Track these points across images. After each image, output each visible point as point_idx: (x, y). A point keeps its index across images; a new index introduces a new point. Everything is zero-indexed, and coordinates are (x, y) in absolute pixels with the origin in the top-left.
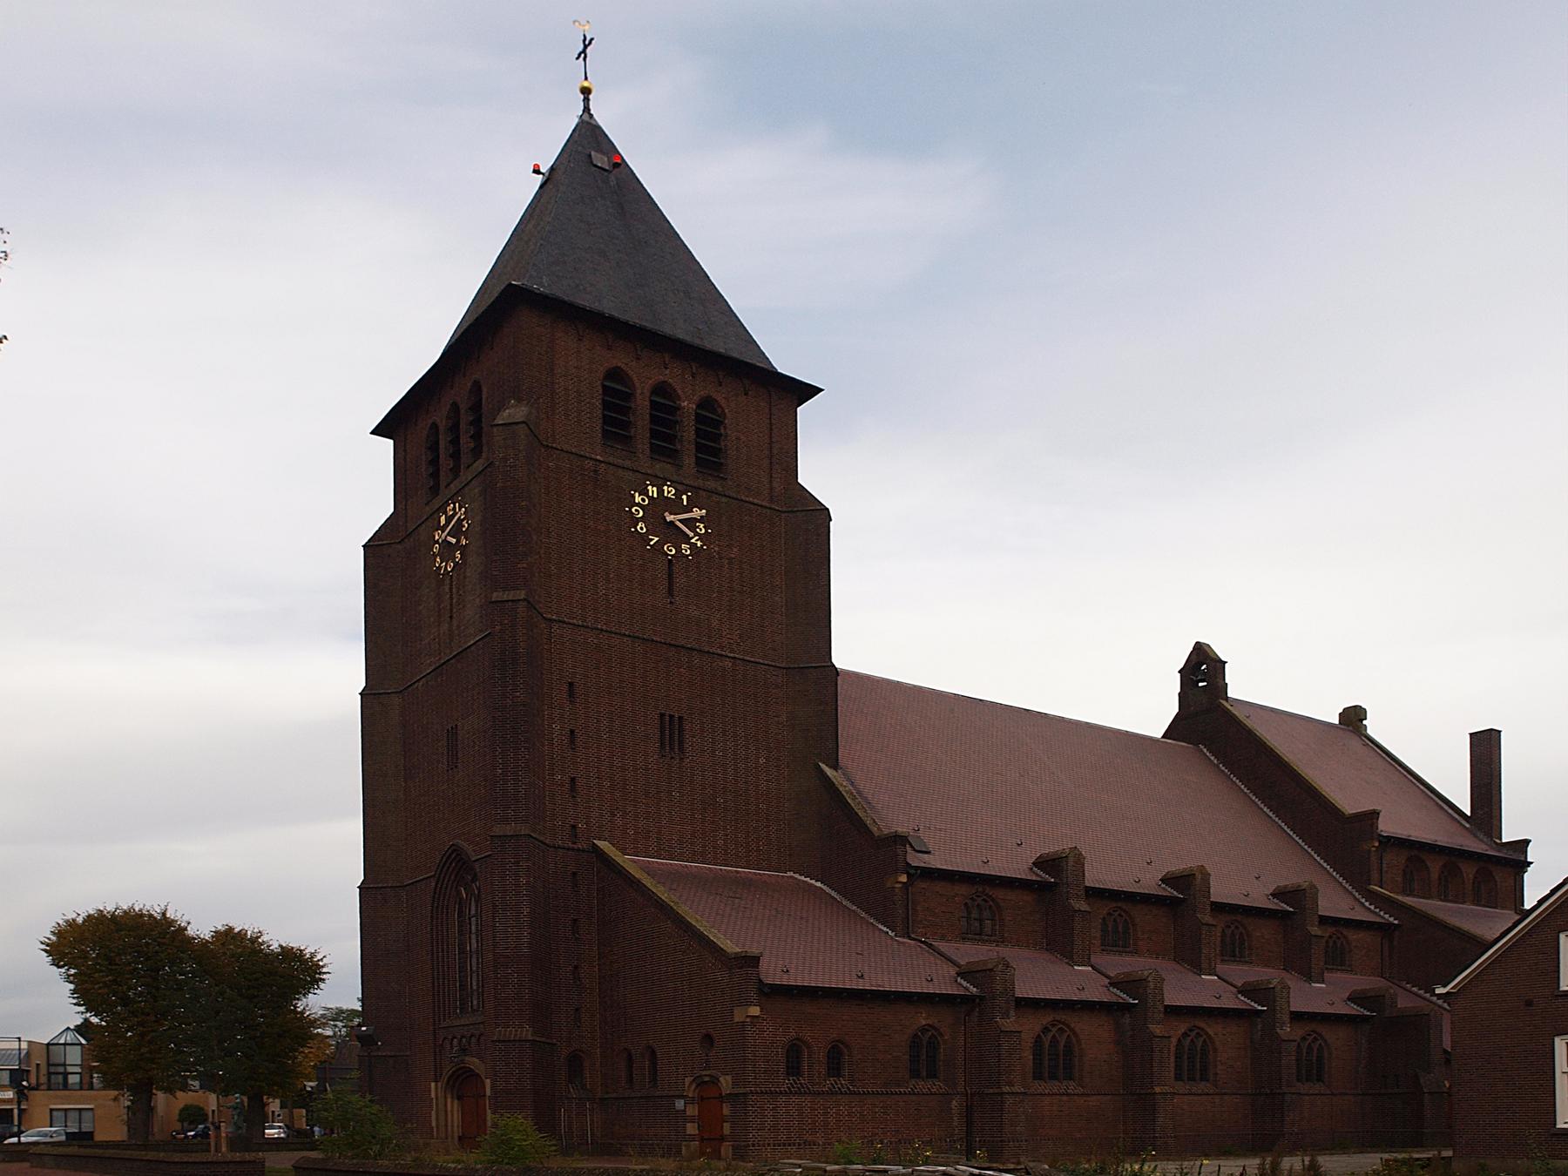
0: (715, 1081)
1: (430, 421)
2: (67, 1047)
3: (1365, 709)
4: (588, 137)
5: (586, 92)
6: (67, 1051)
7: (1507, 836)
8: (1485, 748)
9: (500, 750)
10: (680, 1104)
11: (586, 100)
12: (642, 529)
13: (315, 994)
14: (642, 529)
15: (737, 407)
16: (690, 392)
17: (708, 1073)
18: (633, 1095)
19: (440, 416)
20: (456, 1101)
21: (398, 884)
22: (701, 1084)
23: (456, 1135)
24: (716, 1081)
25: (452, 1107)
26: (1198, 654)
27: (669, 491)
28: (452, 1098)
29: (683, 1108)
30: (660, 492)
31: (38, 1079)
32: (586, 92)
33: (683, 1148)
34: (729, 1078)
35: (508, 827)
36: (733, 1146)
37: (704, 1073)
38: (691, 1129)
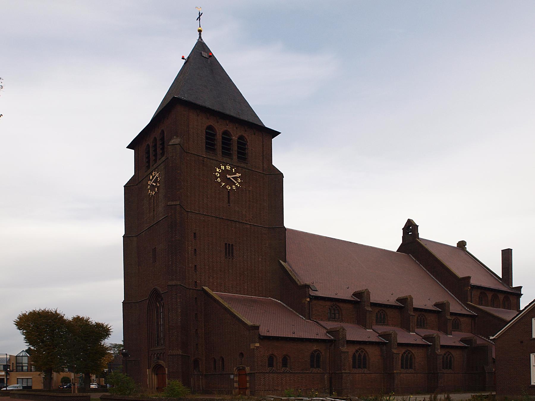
0: (244, 369)
4: (201, 47)
5: (200, 31)
10: (232, 377)
11: (200, 34)
12: (219, 180)
13: (107, 339)
14: (219, 180)
17: (242, 366)
23: (156, 387)
28: (154, 374)
32: (200, 31)
34: (249, 368)
36: (250, 391)
38: (236, 385)
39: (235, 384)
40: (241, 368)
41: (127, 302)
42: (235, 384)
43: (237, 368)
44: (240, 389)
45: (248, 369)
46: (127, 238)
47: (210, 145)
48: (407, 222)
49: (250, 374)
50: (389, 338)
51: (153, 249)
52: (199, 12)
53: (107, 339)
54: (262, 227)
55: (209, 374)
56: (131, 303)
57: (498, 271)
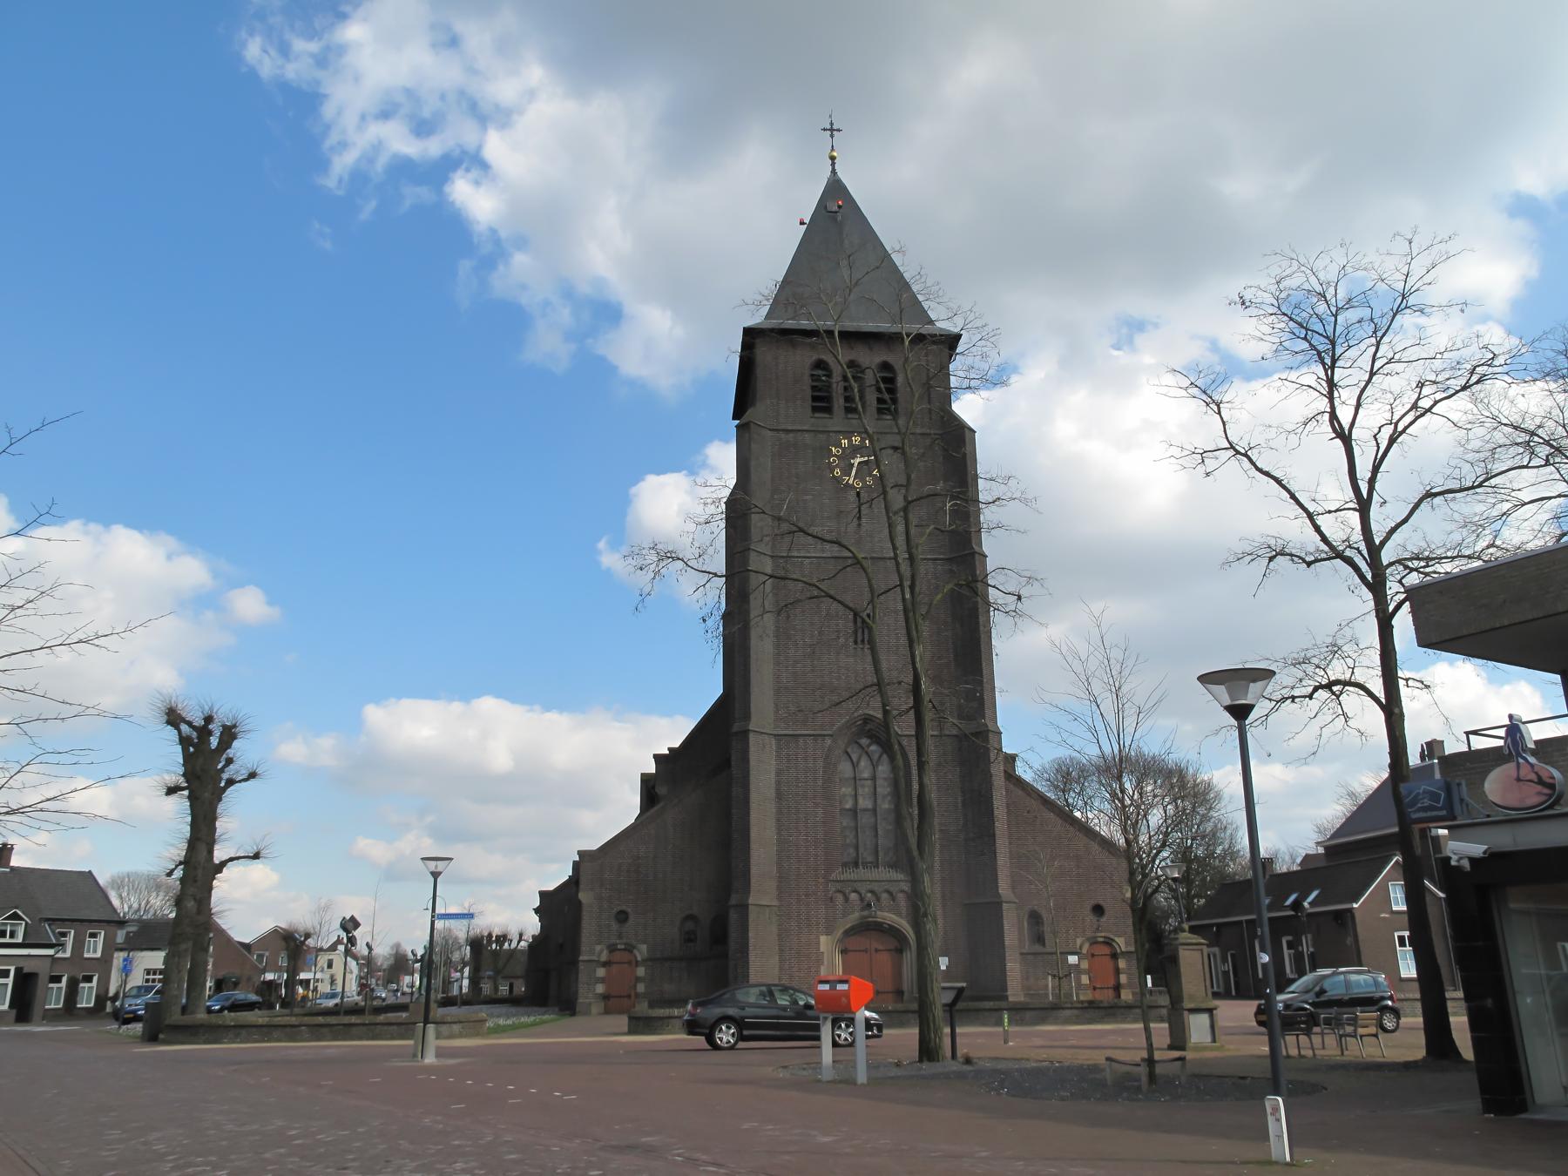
2: (438, 911)
4: (835, 189)
6: (453, 910)
7: (667, 752)
10: (1073, 959)
11: (833, 164)
12: (837, 473)
14: (837, 473)
15: (907, 364)
16: (870, 358)
17: (1103, 934)
22: (1094, 942)
24: (1110, 942)
27: (856, 440)
30: (850, 441)
32: (833, 158)
38: (1085, 979)
44: (1095, 988)
46: (365, 1028)
47: (821, 402)
52: (132, 716)
54: (929, 715)
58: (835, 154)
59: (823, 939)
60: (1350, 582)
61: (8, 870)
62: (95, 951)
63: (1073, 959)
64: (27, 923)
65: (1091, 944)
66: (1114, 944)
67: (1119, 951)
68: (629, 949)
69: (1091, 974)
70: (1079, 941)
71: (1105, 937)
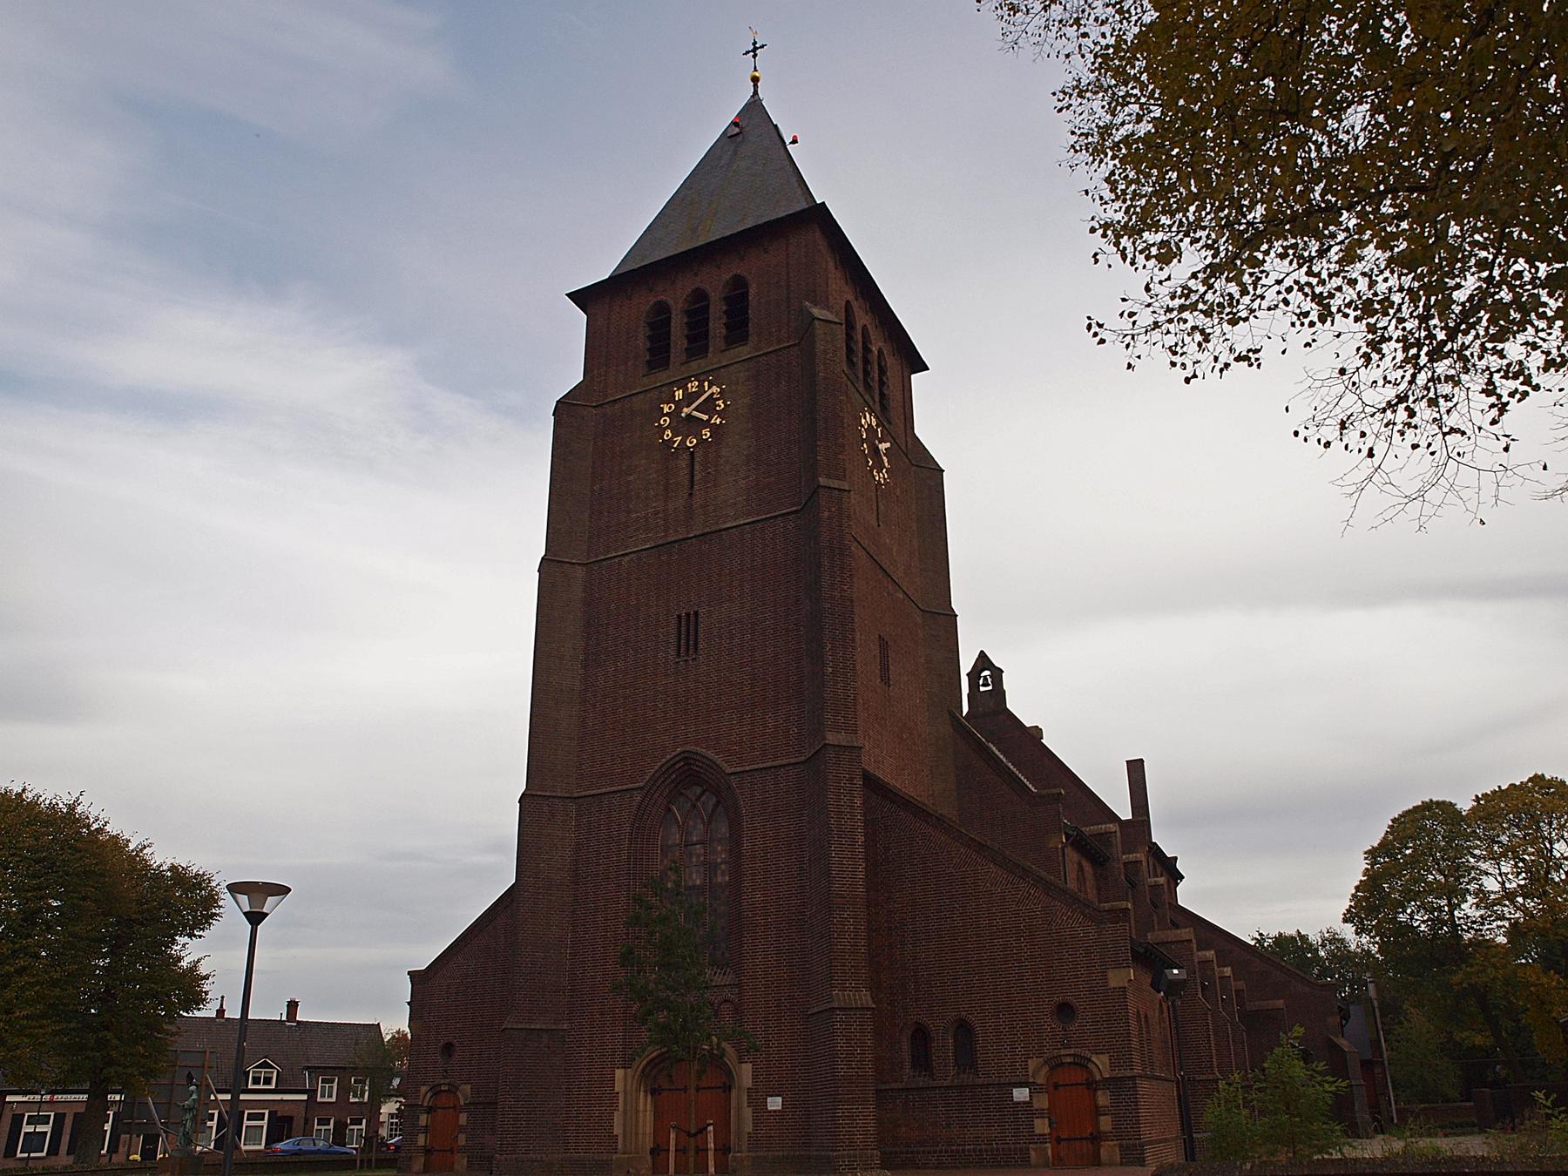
0: (1082, 1063)
1: (653, 300)
3: (1041, 729)
4: (755, 107)
5: (755, 80)
8: (1136, 769)
9: (830, 646)
10: (1021, 1094)
11: (755, 86)
12: (668, 435)
13: (200, 937)
14: (668, 435)
18: (934, 1084)
19: (676, 296)
20: (649, 1097)
21: (567, 795)
22: (1056, 1065)
23: (648, 1148)
25: (645, 1104)
26: (983, 662)
28: (645, 1091)
29: (1028, 1099)
31: (1093, 1062)
32: (755, 80)
33: (1032, 1153)
34: (1105, 1058)
35: (839, 736)
36: (1121, 1146)
37: (1063, 1052)
38: (1041, 1126)
39: (1037, 1122)
40: (1069, 1060)
41: (539, 793)
42: (1037, 1122)
43: (431, 1089)
44: (1059, 1140)
45: (1101, 1064)
48: (977, 659)
49: (1113, 1083)
50: (1209, 973)
51: (679, 617)
53: (200, 937)
55: (894, 1086)
56: (554, 797)
57: (1125, 813)
58: (757, 74)
59: (619, 1073)
60: (1554, 373)
61: (295, 1024)
62: (362, 1095)
63: (1021, 1094)
64: (278, 1071)
65: (1051, 1069)
66: (1090, 1065)
67: (1098, 1077)
68: (453, 1090)
69: (1053, 1119)
70: (1032, 1064)
71: (1074, 1055)
